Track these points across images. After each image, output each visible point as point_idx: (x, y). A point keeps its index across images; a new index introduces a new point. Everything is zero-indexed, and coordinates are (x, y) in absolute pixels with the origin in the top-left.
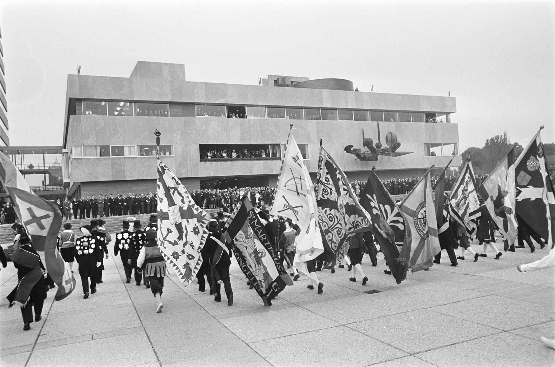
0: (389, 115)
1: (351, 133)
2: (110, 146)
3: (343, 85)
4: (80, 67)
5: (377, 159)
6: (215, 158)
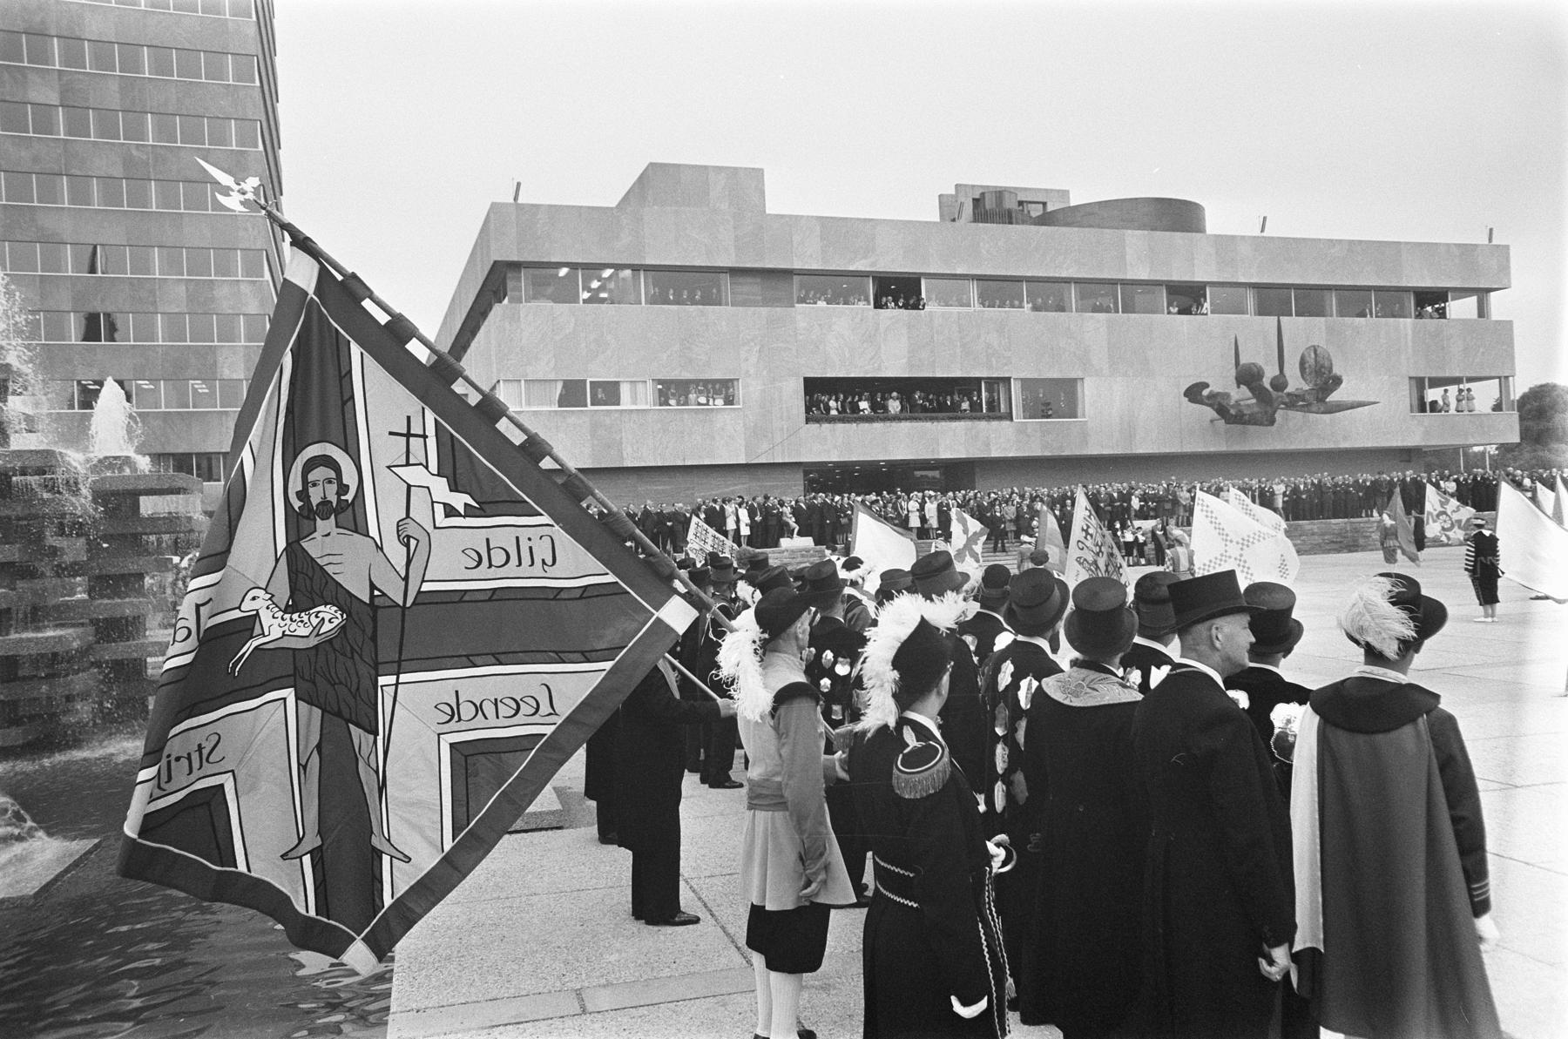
0: (1310, 300)
1: (1205, 347)
3: (1178, 216)
5: (1272, 422)
6: (850, 414)
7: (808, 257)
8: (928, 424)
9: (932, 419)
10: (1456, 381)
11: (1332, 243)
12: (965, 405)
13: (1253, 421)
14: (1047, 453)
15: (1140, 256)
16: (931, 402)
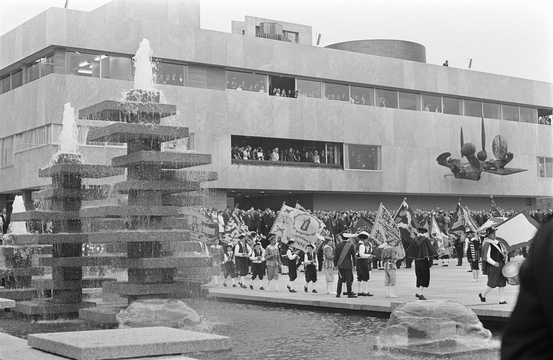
1: (446, 131)
3: (414, 52)
5: (479, 178)
6: (253, 160)
8: (299, 169)
9: (301, 166)
11: (503, 77)
13: (469, 177)
14: (361, 190)
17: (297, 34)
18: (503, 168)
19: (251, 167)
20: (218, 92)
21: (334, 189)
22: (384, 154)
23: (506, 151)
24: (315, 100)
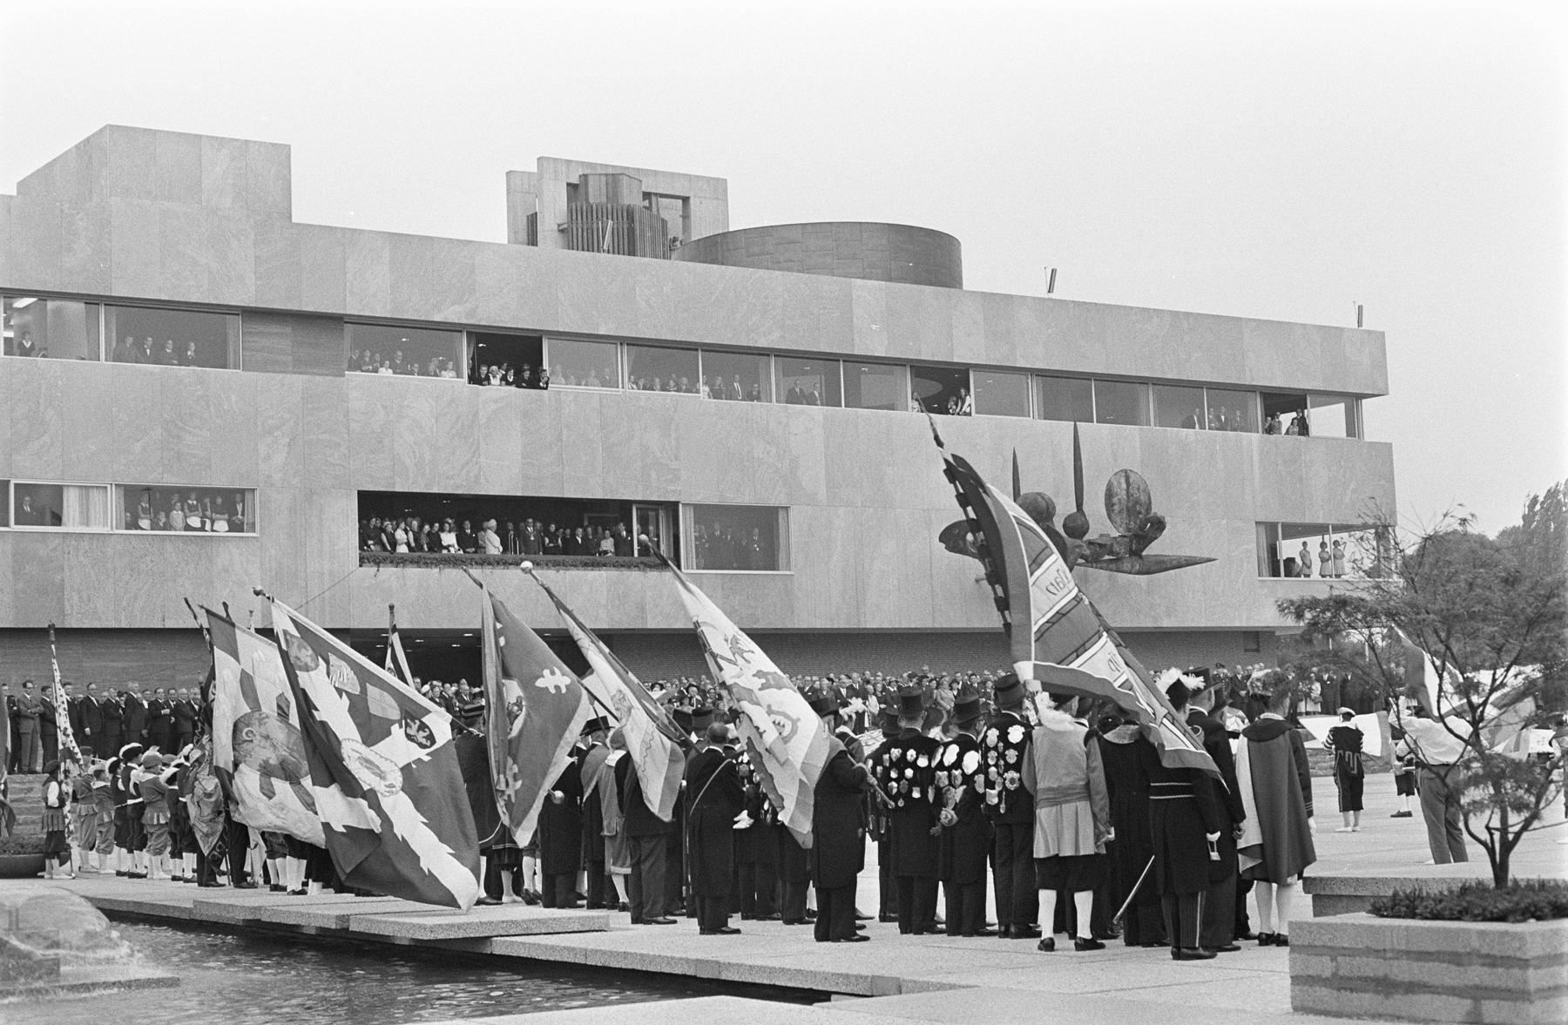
0: (1115, 395)
2: (13, 482)
3: (926, 257)
4: (1360, 308)
6: (428, 552)
7: (370, 293)
9: (557, 565)
10: (1320, 529)
12: (608, 544)
15: (877, 316)
16: (553, 537)
17: (686, 200)
18: (1141, 557)
19: (413, 572)
20: (321, 382)
21: (652, 624)
22: (795, 529)
23: (1149, 509)
24: (596, 390)
